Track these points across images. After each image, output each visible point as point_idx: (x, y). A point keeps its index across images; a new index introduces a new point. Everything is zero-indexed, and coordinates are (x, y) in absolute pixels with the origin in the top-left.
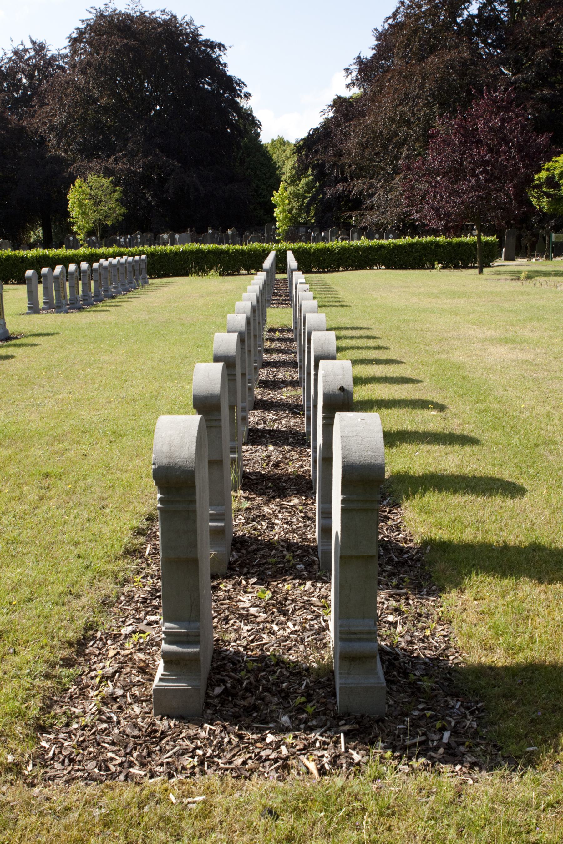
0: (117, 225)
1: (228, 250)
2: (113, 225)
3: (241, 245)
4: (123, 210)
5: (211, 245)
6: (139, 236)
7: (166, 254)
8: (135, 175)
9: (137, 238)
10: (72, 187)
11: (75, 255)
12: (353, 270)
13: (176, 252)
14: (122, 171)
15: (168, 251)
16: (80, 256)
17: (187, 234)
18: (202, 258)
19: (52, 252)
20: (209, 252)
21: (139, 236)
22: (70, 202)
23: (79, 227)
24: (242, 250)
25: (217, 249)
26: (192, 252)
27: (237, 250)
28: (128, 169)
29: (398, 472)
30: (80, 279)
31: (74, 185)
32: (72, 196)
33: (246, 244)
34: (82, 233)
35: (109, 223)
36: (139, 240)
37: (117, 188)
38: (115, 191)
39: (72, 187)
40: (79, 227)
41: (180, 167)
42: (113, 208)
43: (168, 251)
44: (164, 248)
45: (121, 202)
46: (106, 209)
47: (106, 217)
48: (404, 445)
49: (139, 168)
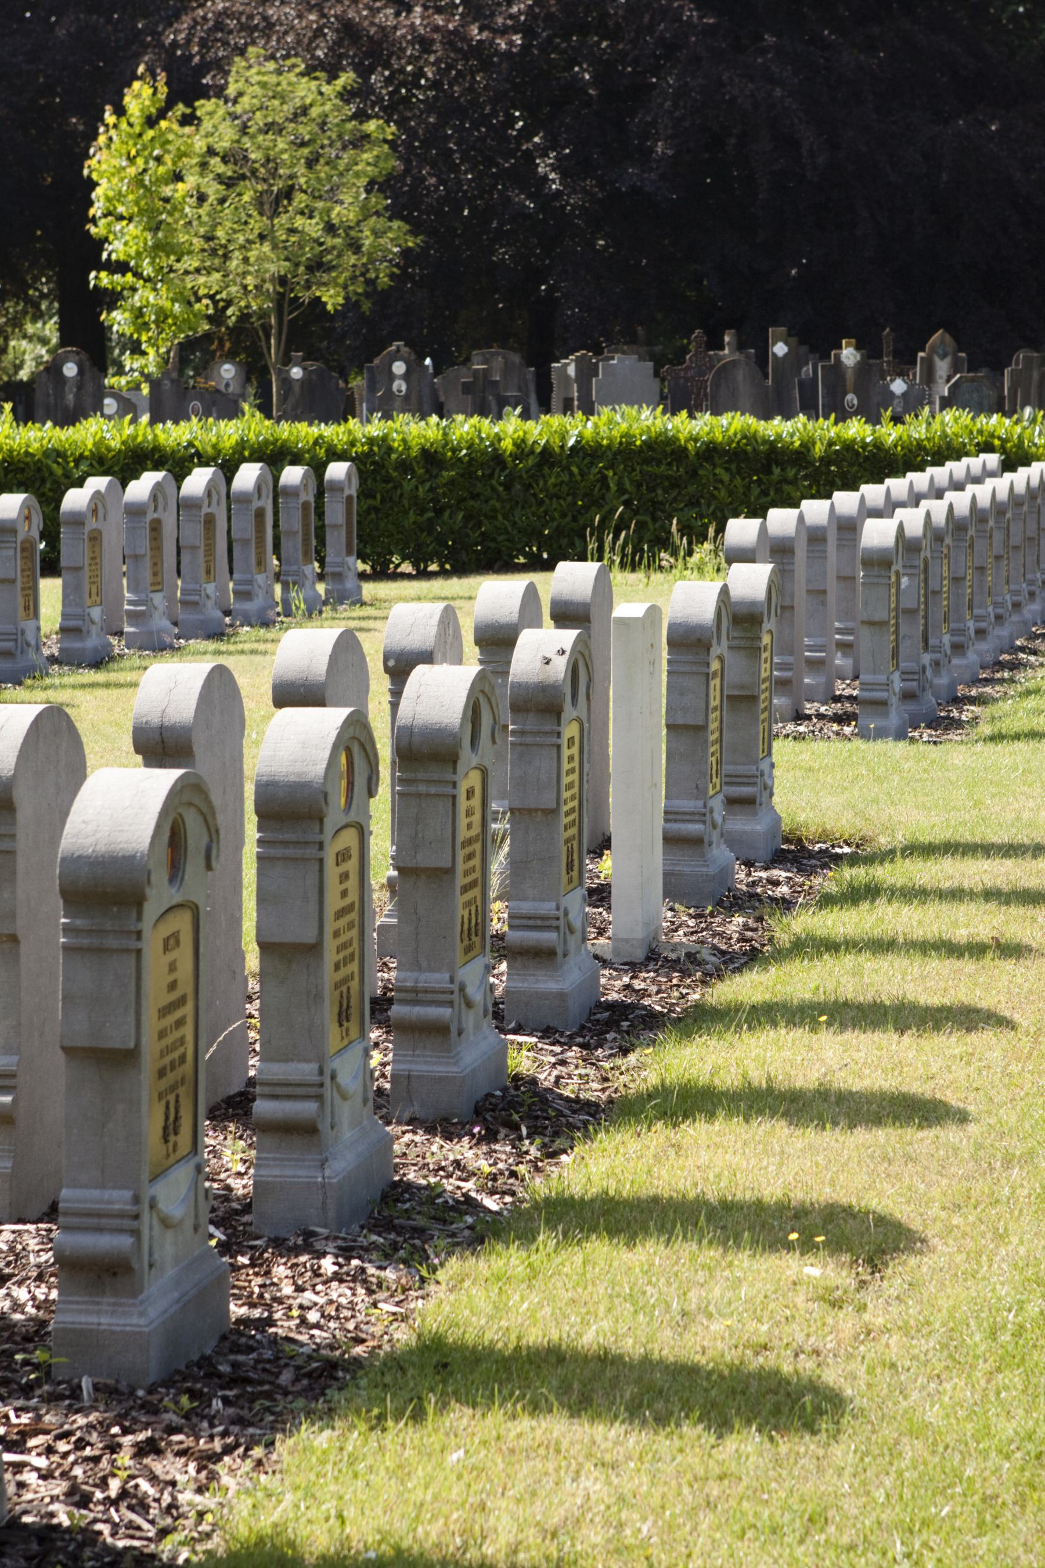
0: (366, 306)
1: (807, 445)
2: (351, 305)
3: (874, 420)
4: (392, 238)
5: (725, 419)
6: (399, 368)
7: (497, 458)
8: (486, 66)
9: (391, 377)
10: (110, 118)
11: (57, 454)
12: (423, 574)
13: (547, 450)
14: (425, 44)
15: (507, 445)
16: (79, 459)
17: (622, 364)
18: (675, 484)
19: (174, 434)
20: (711, 451)
21: (399, 368)
22: (98, 193)
23: (139, 313)
24: (878, 445)
25: (749, 437)
26: (627, 455)
27: (849, 447)
28: (454, 39)
29: (261, 1541)
30: (51, 567)
31: (120, 111)
32: (110, 166)
33: (897, 419)
34: (153, 342)
35: (332, 298)
36: (400, 386)
37: (371, 126)
38: (361, 141)
39: (110, 118)
40: (139, 313)
41: (710, 31)
42: (350, 220)
43: (507, 445)
44: (486, 426)
45: (397, 194)
46: (313, 227)
47: (317, 266)
48: (459, 1416)
49: (504, 31)
